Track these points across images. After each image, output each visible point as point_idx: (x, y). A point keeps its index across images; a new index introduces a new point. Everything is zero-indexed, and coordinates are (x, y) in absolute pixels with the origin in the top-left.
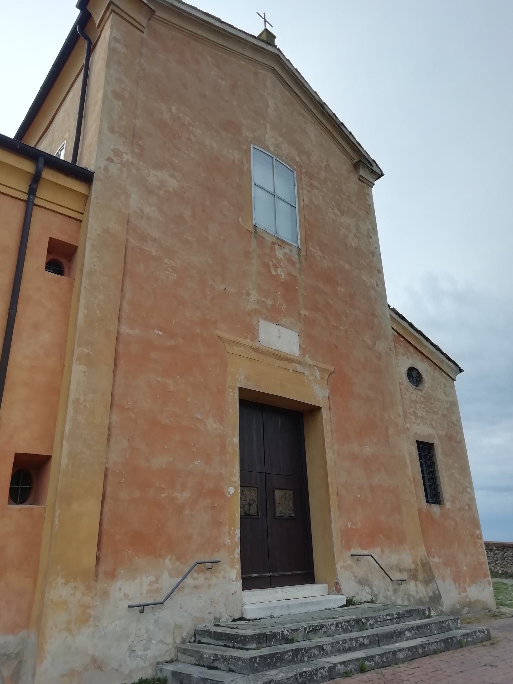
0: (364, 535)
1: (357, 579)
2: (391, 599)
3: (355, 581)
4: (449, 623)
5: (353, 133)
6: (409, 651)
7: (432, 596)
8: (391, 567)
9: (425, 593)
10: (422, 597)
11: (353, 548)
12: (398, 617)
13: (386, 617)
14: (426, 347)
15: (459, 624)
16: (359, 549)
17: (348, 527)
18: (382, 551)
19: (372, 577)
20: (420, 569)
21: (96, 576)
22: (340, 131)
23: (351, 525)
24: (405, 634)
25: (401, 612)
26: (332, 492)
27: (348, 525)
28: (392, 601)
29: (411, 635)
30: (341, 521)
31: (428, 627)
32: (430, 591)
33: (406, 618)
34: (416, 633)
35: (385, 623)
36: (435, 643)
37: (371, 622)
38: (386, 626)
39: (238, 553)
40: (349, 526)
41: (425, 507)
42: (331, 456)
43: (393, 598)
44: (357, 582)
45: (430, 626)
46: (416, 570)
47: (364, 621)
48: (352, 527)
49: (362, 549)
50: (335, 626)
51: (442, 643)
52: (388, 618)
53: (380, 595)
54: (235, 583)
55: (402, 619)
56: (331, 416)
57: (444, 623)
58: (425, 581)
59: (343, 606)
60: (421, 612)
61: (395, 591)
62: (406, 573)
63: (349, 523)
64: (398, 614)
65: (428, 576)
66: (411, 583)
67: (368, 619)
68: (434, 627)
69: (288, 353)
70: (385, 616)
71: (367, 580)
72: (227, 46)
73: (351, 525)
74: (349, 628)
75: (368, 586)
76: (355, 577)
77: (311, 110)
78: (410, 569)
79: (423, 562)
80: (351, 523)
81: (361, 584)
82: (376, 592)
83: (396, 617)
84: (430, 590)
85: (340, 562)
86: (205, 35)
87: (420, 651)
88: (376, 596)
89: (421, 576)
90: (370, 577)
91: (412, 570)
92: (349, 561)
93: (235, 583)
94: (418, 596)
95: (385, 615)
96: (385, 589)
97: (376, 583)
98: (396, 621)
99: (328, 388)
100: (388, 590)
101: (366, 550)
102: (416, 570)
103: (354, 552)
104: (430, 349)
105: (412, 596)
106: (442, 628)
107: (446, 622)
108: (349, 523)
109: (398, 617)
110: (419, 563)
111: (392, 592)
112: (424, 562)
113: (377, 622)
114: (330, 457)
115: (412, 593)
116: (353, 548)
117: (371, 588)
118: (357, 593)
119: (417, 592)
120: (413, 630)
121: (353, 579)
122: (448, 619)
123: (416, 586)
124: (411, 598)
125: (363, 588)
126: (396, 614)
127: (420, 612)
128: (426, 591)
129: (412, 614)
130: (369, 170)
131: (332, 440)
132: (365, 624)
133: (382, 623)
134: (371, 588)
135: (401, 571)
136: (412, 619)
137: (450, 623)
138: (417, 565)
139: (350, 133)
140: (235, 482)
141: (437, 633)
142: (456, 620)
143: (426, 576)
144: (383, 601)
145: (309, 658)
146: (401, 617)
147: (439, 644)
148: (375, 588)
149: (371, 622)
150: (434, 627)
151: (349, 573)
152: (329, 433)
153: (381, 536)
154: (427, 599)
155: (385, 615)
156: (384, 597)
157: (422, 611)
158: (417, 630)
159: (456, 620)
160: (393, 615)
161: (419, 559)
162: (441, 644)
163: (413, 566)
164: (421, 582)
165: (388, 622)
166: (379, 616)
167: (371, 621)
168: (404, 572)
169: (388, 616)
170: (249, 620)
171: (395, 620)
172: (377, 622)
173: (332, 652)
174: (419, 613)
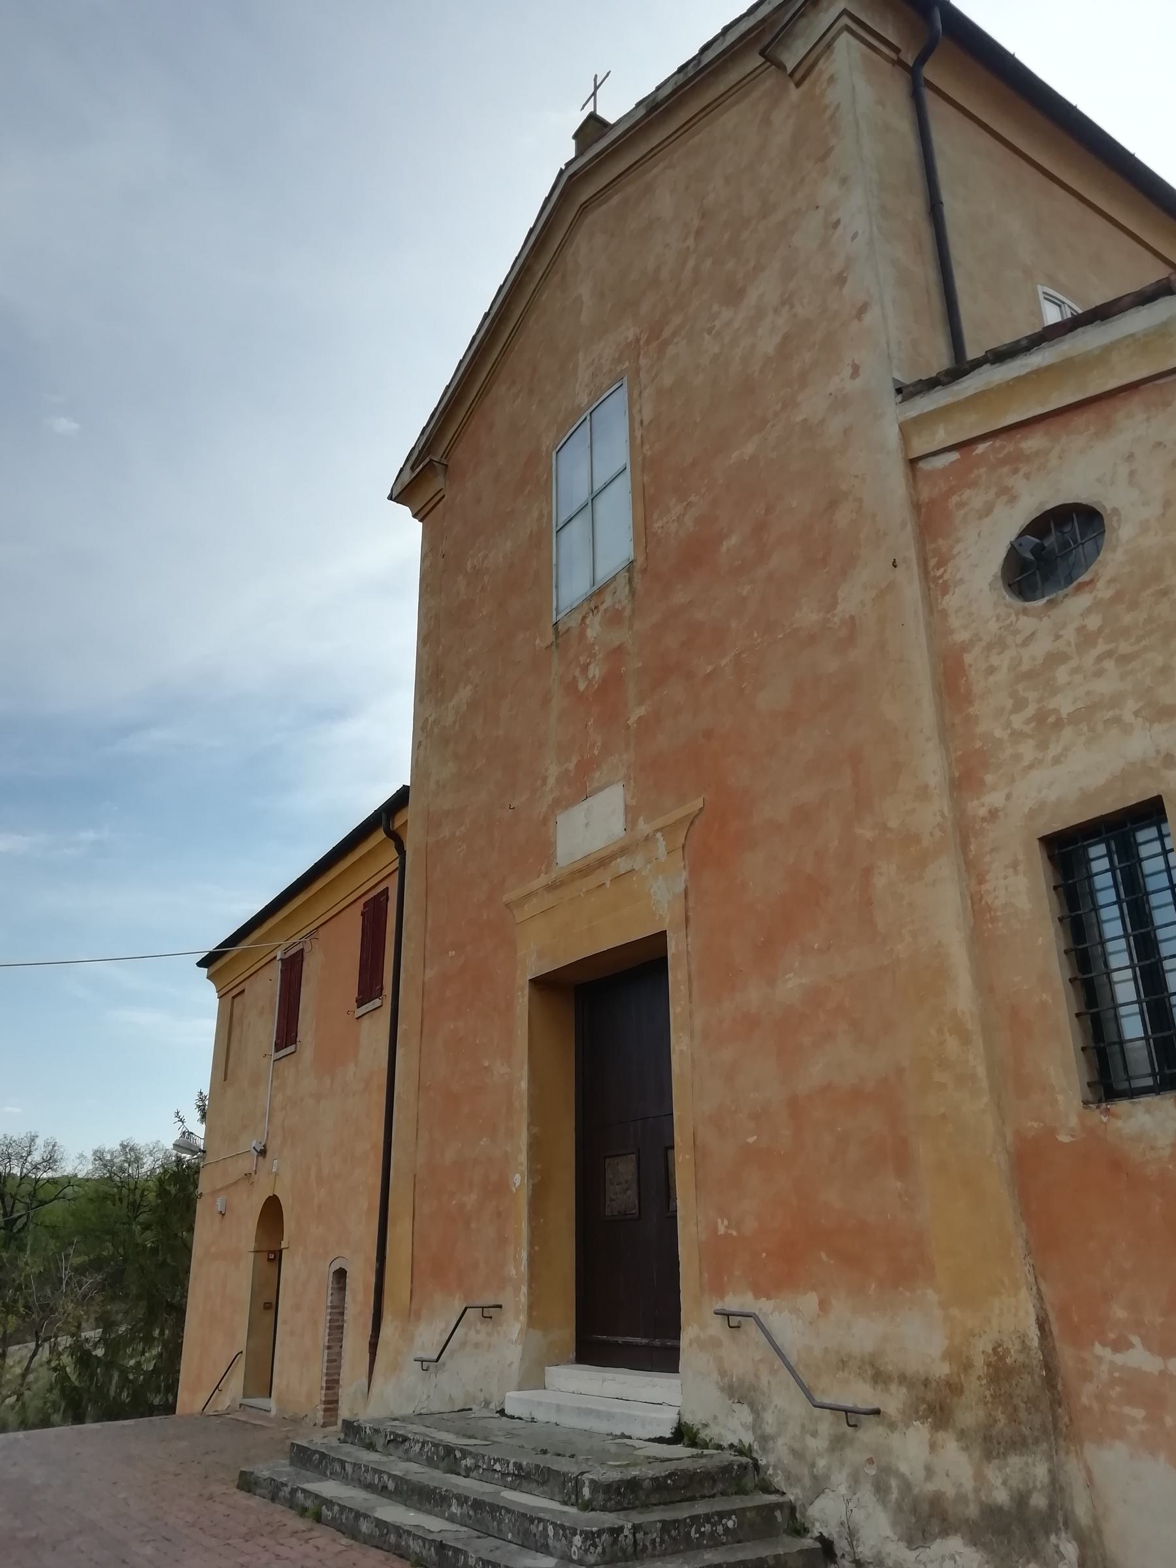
0: (764, 1255)
1: (726, 1380)
2: (813, 1465)
3: (717, 1383)
4: (545, 1529)
5: (727, 22)
6: (376, 1526)
7: (1000, 1509)
8: (843, 1361)
9: (969, 1485)
10: (950, 1492)
11: (731, 1293)
12: (516, 1472)
13: (495, 1463)
14: (1103, 355)
15: (574, 1548)
16: (750, 1295)
17: (719, 1233)
18: (824, 1305)
19: (769, 1383)
20: (975, 1386)
21: (409, 1315)
22: (709, 73)
23: (727, 1227)
24: (450, 1506)
25: (524, 1463)
26: (680, 1144)
27: (719, 1229)
28: (815, 1470)
29: (459, 1512)
30: (699, 1218)
31: (498, 1514)
32: (1004, 1483)
33: (534, 1485)
34: (468, 1513)
35: (490, 1474)
36: (420, 1540)
37: (469, 1462)
38: (491, 1483)
39: (524, 1294)
40: (722, 1230)
41: (1074, 1121)
42: (684, 1048)
43: (821, 1463)
44: (722, 1389)
45: (500, 1514)
46: (954, 1388)
47: (458, 1454)
48: (730, 1231)
49: (757, 1296)
50: (420, 1444)
51: (432, 1549)
52: (498, 1467)
53: (780, 1442)
54: (514, 1346)
55: (525, 1484)
56: (689, 939)
57: (533, 1524)
58: (987, 1439)
59: (660, 1440)
60: (570, 1484)
61: (838, 1444)
62: (904, 1390)
63: (722, 1223)
64: (518, 1466)
65: (1014, 1419)
66: (911, 1431)
67: (465, 1453)
68: (507, 1521)
69: (604, 846)
70: (492, 1461)
71: (753, 1388)
72: (516, 321)
73: (725, 1226)
74: (435, 1459)
75: (752, 1406)
76: (723, 1373)
77: (653, 149)
78: (927, 1379)
79: (1001, 1358)
80: (726, 1222)
81: (731, 1396)
82: (769, 1430)
83: (512, 1472)
84: (1000, 1480)
85: (690, 1327)
86: (489, 366)
87: (393, 1538)
88: (764, 1439)
89: (969, 1415)
90: (765, 1379)
91: (934, 1384)
92: (716, 1326)
93: (514, 1346)
94: (930, 1487)
95: (494, 1459)
96: (803, 1426)
97: (778, 1401)
98: (512, 1481)
99: (684, 866)
100: (814, 1434)
101: (769, 1297)
102: (954, 1388)
103: (733, 1302)
104: (1132, 335)
105: (902, 1477)
106: (527, 1533)
107: (539, 1523)
108: (722, 1223)
109: (516, 1472)
110: (979, 1362)
111: (827, 1443)
112: (1008, 1361)
113: (477, 1467)
114: (681, 1051)
115: (904, 1468)
116: (731, 1293)
117: (757, 1412)
118: (715, 1417)
119: (929, 1472)
120: (466, 1504)
121: (715, 1376)
122: (547, 1518)
123: (933, 1446)
124: (894, 1483)
125: (737, 1407)
126: (515, 1464)
127: (568, 1483)
128: (979, 1476)
129: (548, 1479)
130: (802, 15)
131: (690, 1002)
132: (458, 1460)
133: (485, 1472)
134: (757, 1412)
135: (879, 1378)
136: (544, 1492)
137: (549, 1533)
138: (968, 1366)
139: (726, 30)
140: (522, 1164)
141: (512, 1540)
142: (568, 1531)
143: (1002, 1419)
144: (785, 1462)
145: (331, 1473)
146: (524, 1476)
147: (427, 1546)
148: (769, 1417)
149: (469, 1462)
150: (507, 1521)
151: (708, 1360)
152: (682, 987)
153: (823, 1256)
154: (973, 1511)
155: (494, 1459)
156: (794, 1452)
157: (573, 1482)
158: (472, 1506)
159: (568, 1531)
160: (508, 1466)
161: (983, 1345)
162: (430, 1549)
163: (943, 1370)
164: (962, 1435)
165: (496, 1476)
166: (483, 1456)
167: (468, 1459)
168: (893, 1387)
169: (498, 1463)
170: (512, 1417)
171: (509, 1479)
172: (477, 1467)
173: (352, 1479)
174: (564, 1484)
